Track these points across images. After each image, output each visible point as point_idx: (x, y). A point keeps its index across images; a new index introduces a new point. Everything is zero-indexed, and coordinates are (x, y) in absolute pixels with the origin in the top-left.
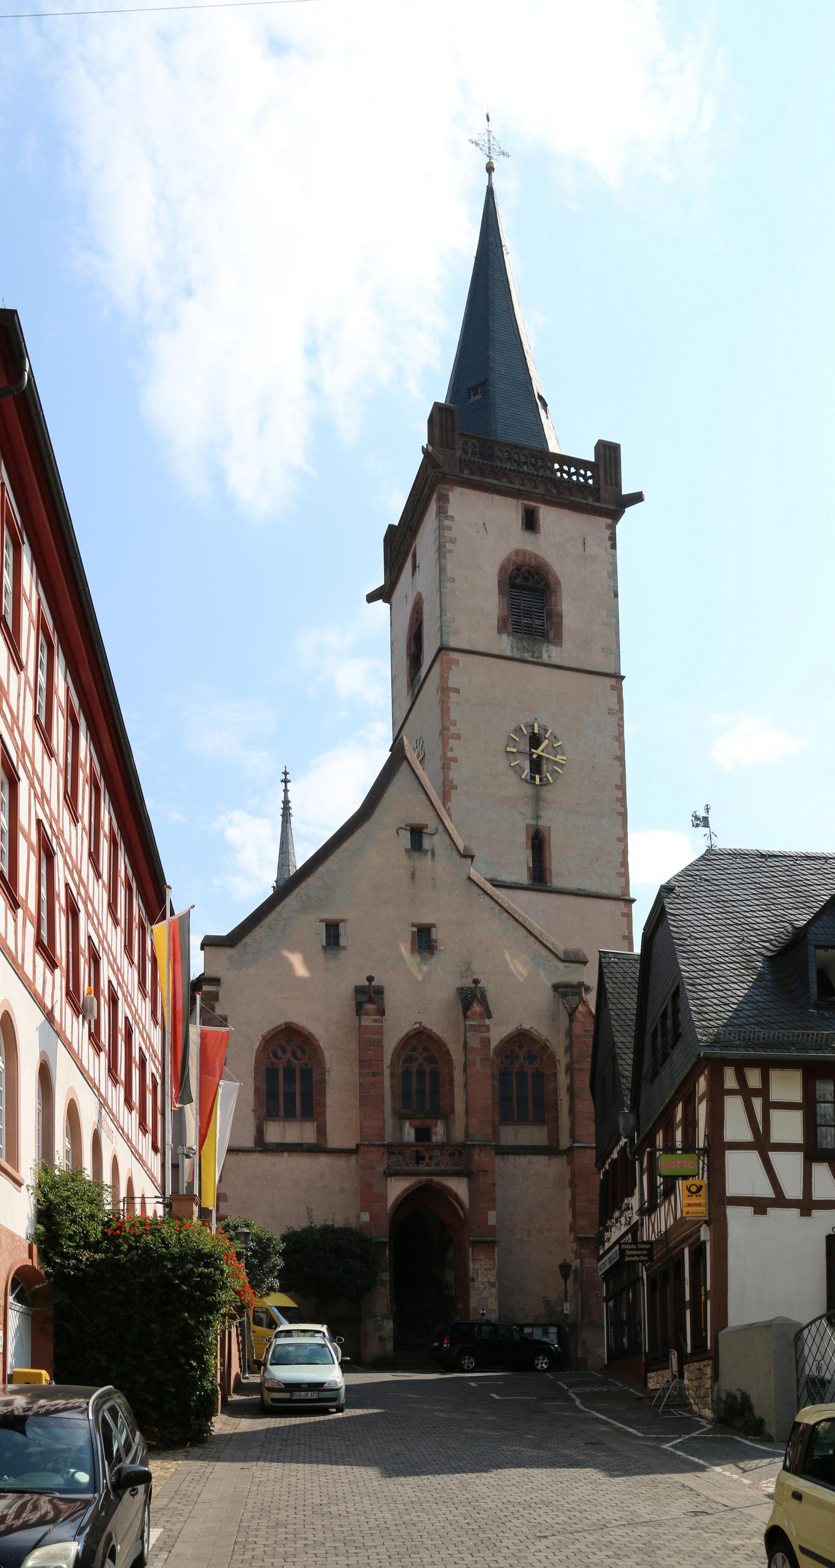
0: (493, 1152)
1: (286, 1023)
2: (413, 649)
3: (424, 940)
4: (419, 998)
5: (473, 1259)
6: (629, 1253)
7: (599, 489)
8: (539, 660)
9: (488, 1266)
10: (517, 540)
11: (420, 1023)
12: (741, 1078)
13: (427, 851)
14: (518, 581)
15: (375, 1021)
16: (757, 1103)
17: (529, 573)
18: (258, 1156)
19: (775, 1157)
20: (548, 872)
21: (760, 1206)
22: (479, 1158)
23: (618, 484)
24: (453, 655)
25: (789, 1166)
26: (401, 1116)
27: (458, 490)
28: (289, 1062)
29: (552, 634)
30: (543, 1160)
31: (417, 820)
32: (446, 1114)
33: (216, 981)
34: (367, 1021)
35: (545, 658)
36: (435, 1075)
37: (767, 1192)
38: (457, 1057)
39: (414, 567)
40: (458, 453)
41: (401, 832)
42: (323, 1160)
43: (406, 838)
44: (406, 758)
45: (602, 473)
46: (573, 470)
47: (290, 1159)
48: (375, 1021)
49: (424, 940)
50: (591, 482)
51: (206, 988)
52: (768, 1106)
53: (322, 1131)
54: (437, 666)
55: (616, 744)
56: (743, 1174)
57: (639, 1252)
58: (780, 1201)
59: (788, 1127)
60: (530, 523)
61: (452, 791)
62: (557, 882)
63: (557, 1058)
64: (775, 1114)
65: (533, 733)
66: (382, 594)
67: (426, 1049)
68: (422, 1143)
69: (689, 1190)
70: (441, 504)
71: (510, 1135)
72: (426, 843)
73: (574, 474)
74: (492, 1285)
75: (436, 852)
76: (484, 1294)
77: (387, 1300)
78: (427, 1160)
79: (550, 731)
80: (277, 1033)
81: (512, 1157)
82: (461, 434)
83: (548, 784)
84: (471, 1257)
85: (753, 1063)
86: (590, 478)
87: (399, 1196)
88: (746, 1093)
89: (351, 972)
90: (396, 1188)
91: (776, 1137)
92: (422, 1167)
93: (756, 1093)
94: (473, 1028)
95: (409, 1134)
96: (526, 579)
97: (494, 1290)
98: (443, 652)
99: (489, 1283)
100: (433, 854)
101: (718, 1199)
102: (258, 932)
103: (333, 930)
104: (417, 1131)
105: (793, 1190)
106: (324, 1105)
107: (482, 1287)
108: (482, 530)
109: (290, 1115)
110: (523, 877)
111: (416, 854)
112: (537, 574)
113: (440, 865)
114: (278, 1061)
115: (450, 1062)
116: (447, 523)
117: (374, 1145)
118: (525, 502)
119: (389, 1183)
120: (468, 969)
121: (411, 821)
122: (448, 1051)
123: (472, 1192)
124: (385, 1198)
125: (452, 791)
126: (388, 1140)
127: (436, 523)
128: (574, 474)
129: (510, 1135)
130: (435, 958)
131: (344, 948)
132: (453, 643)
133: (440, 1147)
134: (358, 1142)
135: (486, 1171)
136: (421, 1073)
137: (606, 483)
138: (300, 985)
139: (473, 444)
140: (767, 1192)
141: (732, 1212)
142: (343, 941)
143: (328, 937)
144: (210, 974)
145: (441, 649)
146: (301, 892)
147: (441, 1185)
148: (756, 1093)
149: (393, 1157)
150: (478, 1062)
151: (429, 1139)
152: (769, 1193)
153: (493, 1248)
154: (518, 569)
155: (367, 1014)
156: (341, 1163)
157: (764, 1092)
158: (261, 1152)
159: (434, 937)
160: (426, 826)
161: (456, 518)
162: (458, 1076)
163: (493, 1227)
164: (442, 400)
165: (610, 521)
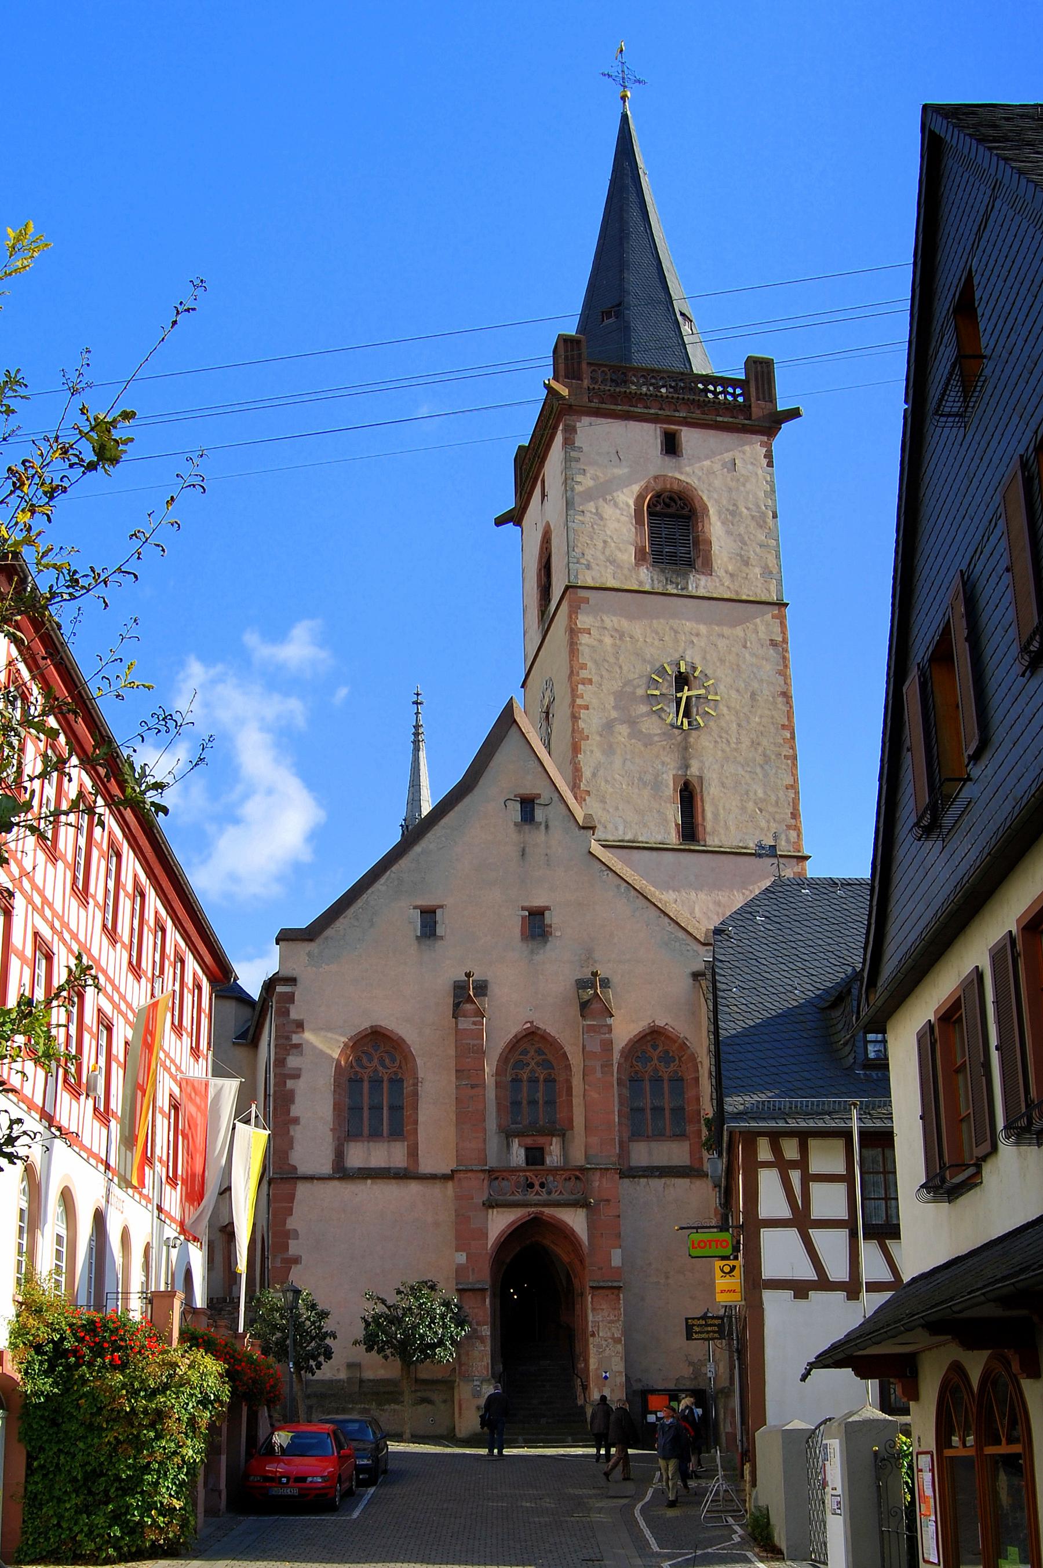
0: (617, 1176)
1: (372, 1027)
2: (544, 579)
3: (536, 925)
4: (525, 995)
5: (593, 1309)
6: (697, 1329)
7: (750, 406)
8: (684, 593)
9: (612, 1317)
10: (657, 463)
11: (532, 1023)
12: (776, 1150)
13: (540, 823)
14: (658, 509)
15: (474, 1023)
16: (795, 1176)
17: (671, 498)
18: (336, 1183)
19: (817, 1235)
20: (700, 828)
21: (800, 1289)
22: (599, 1184)
23: (771, 398)
24: (582, 593)
25: (832, 1245)
26: (508, 1135)
27: (586, 420)
28: (376, 1071)
29: (699, 562)
30: (682, 1184)
31: (527, 790)
32: (562, 1131)
33: (292, 981)
34: (465, 1024)
35: (691, 589)
36: (550, 1081)
37: (809, 1273)
38: (576, 1060)
39: (544, 495)
40: (586, 383)
41: (509, 803)
42: (414, 1187)
43: (515, 810)
44: (515, 721)
45: (753, 390)
46: (719, 389)
47: (375, 1187)
48: (474, 1023)
49: (536, 925)
50: (740, 399)
51: (279, 989)
52: (807, 1179)
53: (413, 1153)
54: (565, 603)
55: (781, 679)
56: (781, 1254)
57: (709, 1329)
58: (824, 1283)
59: (829, 1201)
60: (671, 446)
61: (583, 742)
62: (713, 841)
63: (699, 1059)
64: (815, 1188)
65: (679, 672)
66: (514, 517)
67: (539, 1052)
68: (533, 1167)
69: (722, 1271)
70: (568, 435)
71: (642, 1154)
72: (539, 814)
73: (720, 393)
74: (617, 1341)
75: (550, 824)
76: (607, 1352)
77: (488, 1360)
78: (537, 1187)
79: (699, 669)
80: (362, 1038)
81: (643, 1181)
82: (588, 363)
83: (698, 727)
84: (590, 1305)
85: (790, 1134)
86: (739, 395)
87: (503, 1232)
88: (782, 1166)
89: (449, 965)
90: (499, 1223)
91: (816, 1214)
92: (532, 1197)
93: (794, 1164)
94: (591, 1029)
95: (518, 1155)
96: (668, 506)
97: (620, 1348)
98: (570, 590)
99: (613, 1338)
100: (547, 827)
101: (755, 1283)
102: (341, 924)
103: (429, 916)
104: (528, 1150)
105: (838, 1270)
106: (416, 1122)
107: (604, 1343)
108: (615, 458)
109: (375, 1135)
110: (673, 838)
111: (527, 827)
112: (681, 499)
113: (553, 840)
114: (362, 1071)
115: (568, 1067)
116: (573, 454)
117: (472, 1170)
118: (665, 426)
119: (490, 1217)
120: (589, 956)
121: (522, 791)
122: (565, 1054)
123: (591, 1226)
124: (486, 1236)
125: (583, 742)
126: (492, 1162)
127: (562, 455)
128: (720, 393)
129: (642, 1154)
130: (549, 946)
131: (442, 938)
132: (587, 579)
133: (554, 1171)
134: (454, 1166)
135: (608, 1201)
136: (533, 1081)
137: (758, 399)
138: (387, 989)
139: (603, 372)
140: (809, 1273)
141: (768, 1295)
142: (440, 931)
143: (423, 926)
144: (285, 973)
145: (567, 588)
146: (393, 875)
147: (553, 1217)
148: (794, 1164)
149: (496, 1183)
150: (598, 1068)
151: (543, 1163)
152: (811, 1275)
153: (618, 1295)
154: (658, 496)
155: (465, 1016)
156: (436, 1191)
157: (802, 1164)
158: (339, 1179)
159: (547, 921)
160: (539, 796)
161: (584, 449)
162: (577, 1082)
163: (618, 1268)
164: (571, 329)
165: (765, 438)
